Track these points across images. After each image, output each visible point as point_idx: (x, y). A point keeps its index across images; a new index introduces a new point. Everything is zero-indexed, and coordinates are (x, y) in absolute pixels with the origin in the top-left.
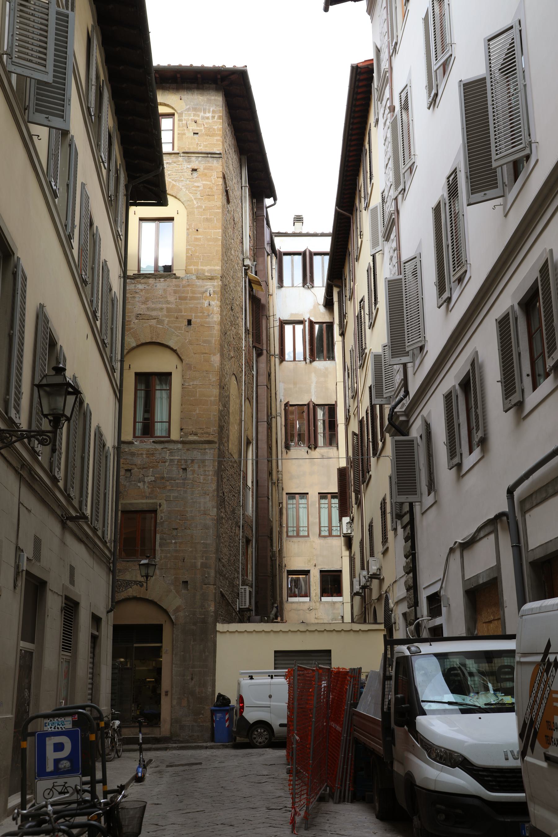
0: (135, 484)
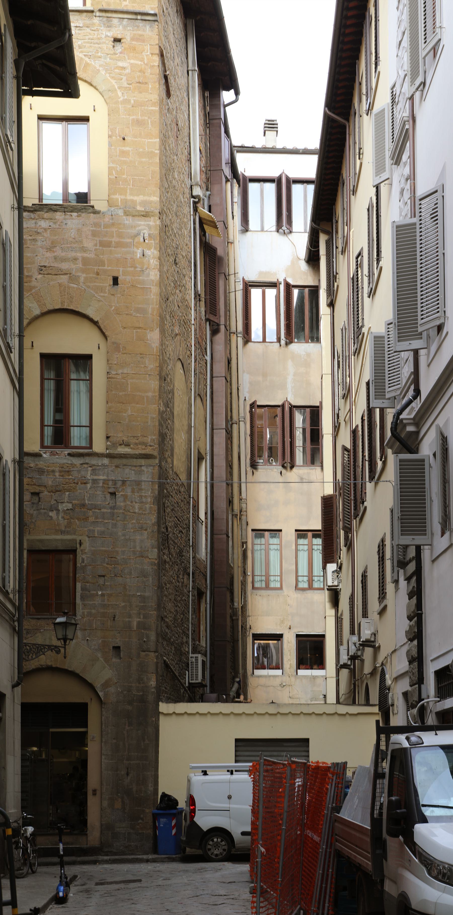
0: (45, 513)
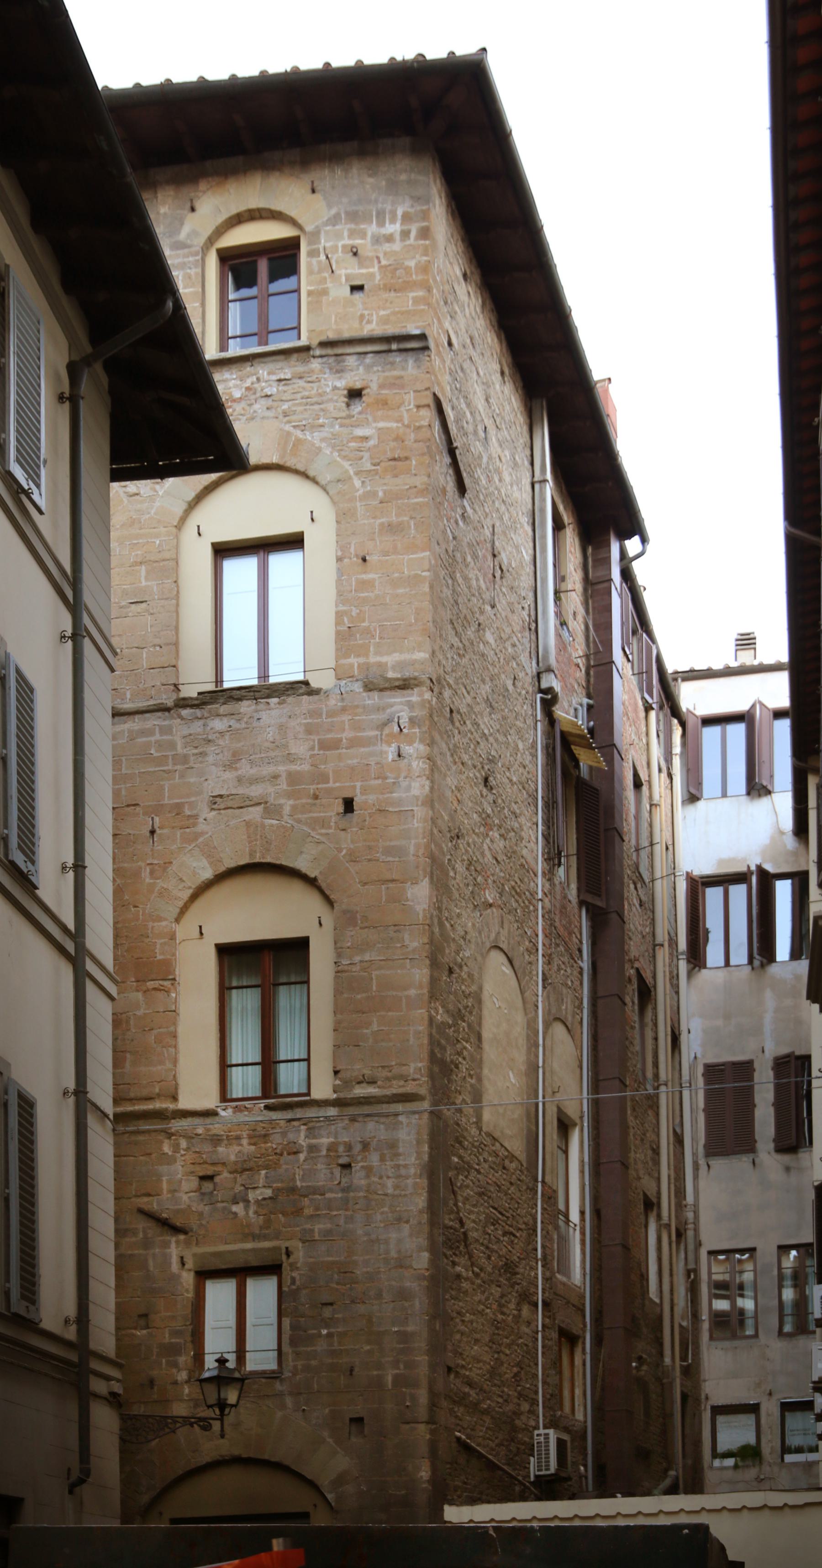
0: (224, 1208)
